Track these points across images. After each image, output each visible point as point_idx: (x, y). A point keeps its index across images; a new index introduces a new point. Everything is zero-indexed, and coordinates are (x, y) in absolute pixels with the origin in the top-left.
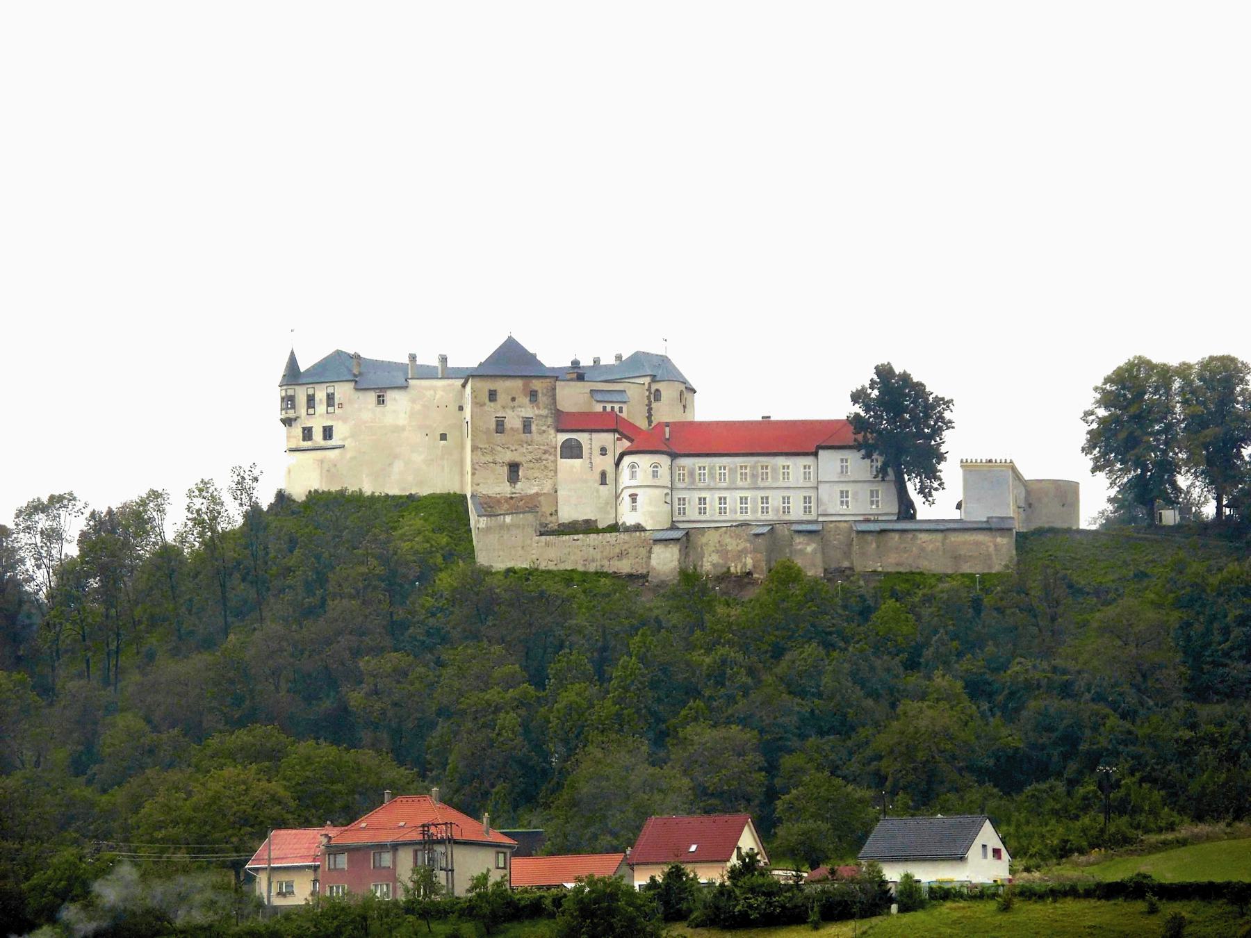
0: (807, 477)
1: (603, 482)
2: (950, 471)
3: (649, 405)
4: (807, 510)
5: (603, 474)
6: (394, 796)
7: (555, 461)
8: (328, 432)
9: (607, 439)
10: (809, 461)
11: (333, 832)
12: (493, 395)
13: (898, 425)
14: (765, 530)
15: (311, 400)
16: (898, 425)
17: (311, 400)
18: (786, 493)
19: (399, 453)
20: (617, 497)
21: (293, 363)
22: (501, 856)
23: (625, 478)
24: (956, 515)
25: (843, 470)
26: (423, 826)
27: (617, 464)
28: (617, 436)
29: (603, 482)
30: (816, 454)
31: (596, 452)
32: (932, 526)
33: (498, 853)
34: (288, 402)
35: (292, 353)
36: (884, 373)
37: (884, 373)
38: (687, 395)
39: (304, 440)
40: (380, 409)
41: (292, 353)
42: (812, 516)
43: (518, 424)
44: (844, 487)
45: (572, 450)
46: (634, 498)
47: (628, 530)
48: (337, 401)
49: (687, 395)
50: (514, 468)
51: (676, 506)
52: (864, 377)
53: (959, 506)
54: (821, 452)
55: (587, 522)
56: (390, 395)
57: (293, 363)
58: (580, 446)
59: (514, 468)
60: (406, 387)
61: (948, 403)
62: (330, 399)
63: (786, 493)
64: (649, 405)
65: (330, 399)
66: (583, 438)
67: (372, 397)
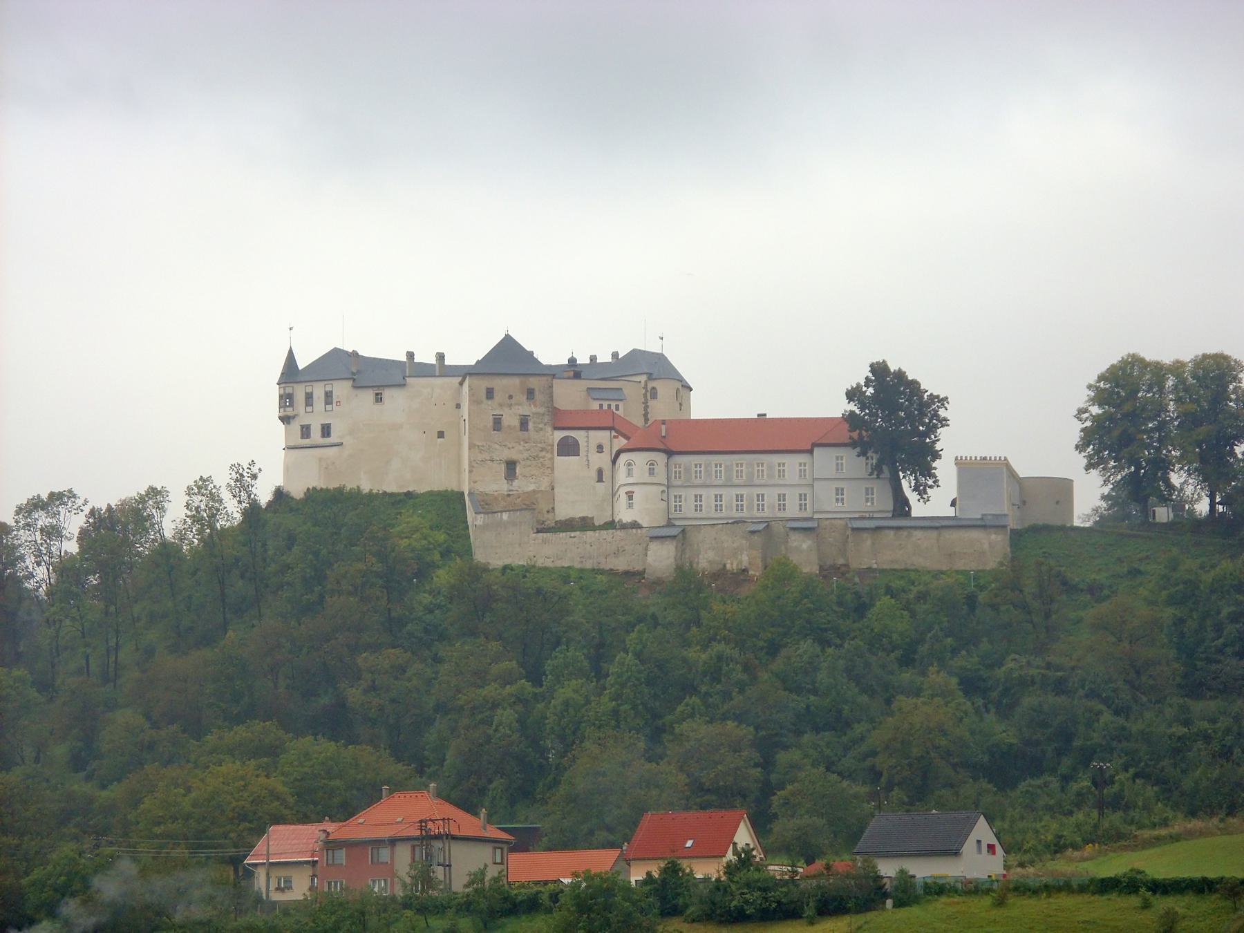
0: (802, 474)
1: (600, 480)
2: (945, 468)
3: (645, 403)
4: (802, 507)
5: (600, 472)
6: (391, 792)
7: (552, 459)
8: (326, 430)
9: (603, 436)
10: (803, 458)
11: (331, 827)
12: (490, 393)
13: (893, 421)
14: (761, 527)
15: (309, 397)
16: (893, 421)
17: (309, 397)
18: (327, 441)
19: (399, 456)
20: (613, 495)
21: (291, 357)
22: (498, 852)
23: (622, 476)
24: (951, 512)
25: (838, 467)
26: (421, 822)
27: (614, 462)
28: (614, 433)
29: (600, 480)
30: (811, 452)
31: (593, 448)
32: (927, 524)
33: (495, 848)
34: (286, 399)
35: (291, 352)
36: (879, 370)
37: (879, 370)
38: (683, 392)
39: (302, 437)
40: (378, 406)
41: (291, 352)
42: (808, 514)
43: (516, 423)
44: (840, 485)
45: (569, 448)
46: (630, 496)
47: (624, 527)
48: (335, 400)
49: (683, 392)
50: (511, 466)
51: (673, 504)
52: (860, 374)
53: (953, 504)
54: (817, 451)
55: (583, 519)
56: (387, 394)
57: (291, 357)
58: (576, 444)
59: (511, 466)
60: (402, 385)
61: (943, 401)
62: (328, 396)
63: (327, 441)
64: (645, 403)
65: (328, 396)
66: (579, 435)
67: (369, 395)
